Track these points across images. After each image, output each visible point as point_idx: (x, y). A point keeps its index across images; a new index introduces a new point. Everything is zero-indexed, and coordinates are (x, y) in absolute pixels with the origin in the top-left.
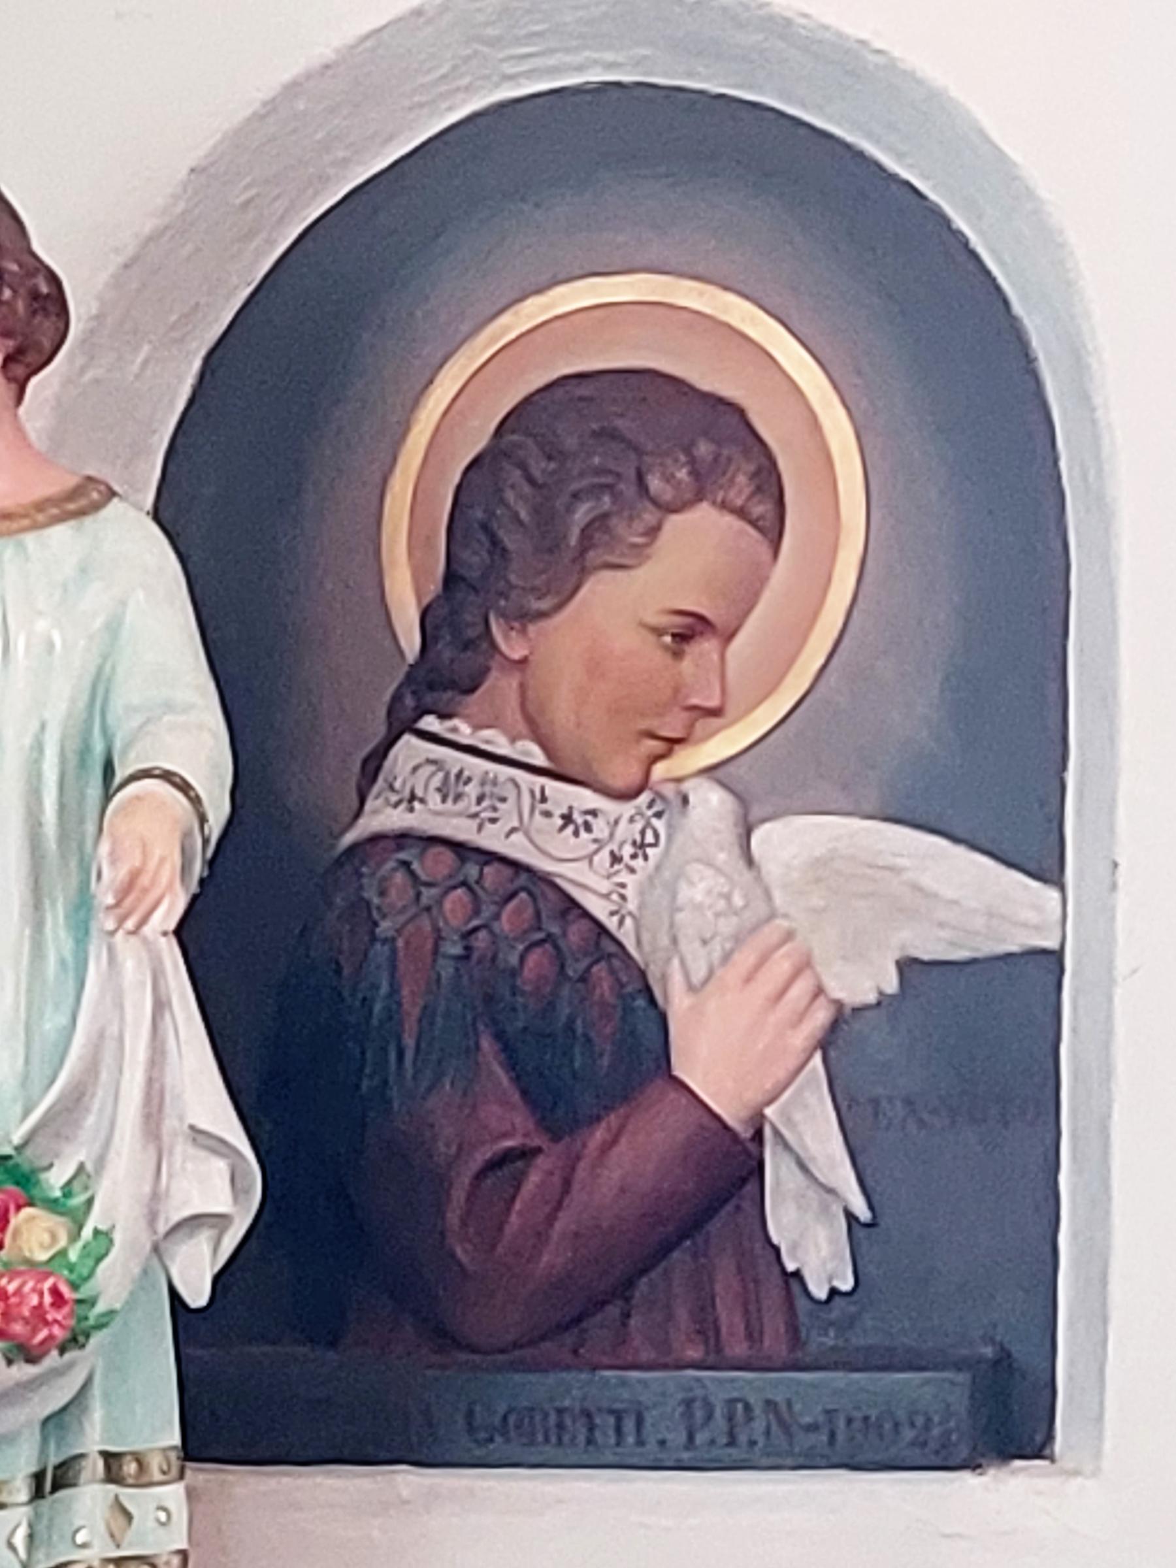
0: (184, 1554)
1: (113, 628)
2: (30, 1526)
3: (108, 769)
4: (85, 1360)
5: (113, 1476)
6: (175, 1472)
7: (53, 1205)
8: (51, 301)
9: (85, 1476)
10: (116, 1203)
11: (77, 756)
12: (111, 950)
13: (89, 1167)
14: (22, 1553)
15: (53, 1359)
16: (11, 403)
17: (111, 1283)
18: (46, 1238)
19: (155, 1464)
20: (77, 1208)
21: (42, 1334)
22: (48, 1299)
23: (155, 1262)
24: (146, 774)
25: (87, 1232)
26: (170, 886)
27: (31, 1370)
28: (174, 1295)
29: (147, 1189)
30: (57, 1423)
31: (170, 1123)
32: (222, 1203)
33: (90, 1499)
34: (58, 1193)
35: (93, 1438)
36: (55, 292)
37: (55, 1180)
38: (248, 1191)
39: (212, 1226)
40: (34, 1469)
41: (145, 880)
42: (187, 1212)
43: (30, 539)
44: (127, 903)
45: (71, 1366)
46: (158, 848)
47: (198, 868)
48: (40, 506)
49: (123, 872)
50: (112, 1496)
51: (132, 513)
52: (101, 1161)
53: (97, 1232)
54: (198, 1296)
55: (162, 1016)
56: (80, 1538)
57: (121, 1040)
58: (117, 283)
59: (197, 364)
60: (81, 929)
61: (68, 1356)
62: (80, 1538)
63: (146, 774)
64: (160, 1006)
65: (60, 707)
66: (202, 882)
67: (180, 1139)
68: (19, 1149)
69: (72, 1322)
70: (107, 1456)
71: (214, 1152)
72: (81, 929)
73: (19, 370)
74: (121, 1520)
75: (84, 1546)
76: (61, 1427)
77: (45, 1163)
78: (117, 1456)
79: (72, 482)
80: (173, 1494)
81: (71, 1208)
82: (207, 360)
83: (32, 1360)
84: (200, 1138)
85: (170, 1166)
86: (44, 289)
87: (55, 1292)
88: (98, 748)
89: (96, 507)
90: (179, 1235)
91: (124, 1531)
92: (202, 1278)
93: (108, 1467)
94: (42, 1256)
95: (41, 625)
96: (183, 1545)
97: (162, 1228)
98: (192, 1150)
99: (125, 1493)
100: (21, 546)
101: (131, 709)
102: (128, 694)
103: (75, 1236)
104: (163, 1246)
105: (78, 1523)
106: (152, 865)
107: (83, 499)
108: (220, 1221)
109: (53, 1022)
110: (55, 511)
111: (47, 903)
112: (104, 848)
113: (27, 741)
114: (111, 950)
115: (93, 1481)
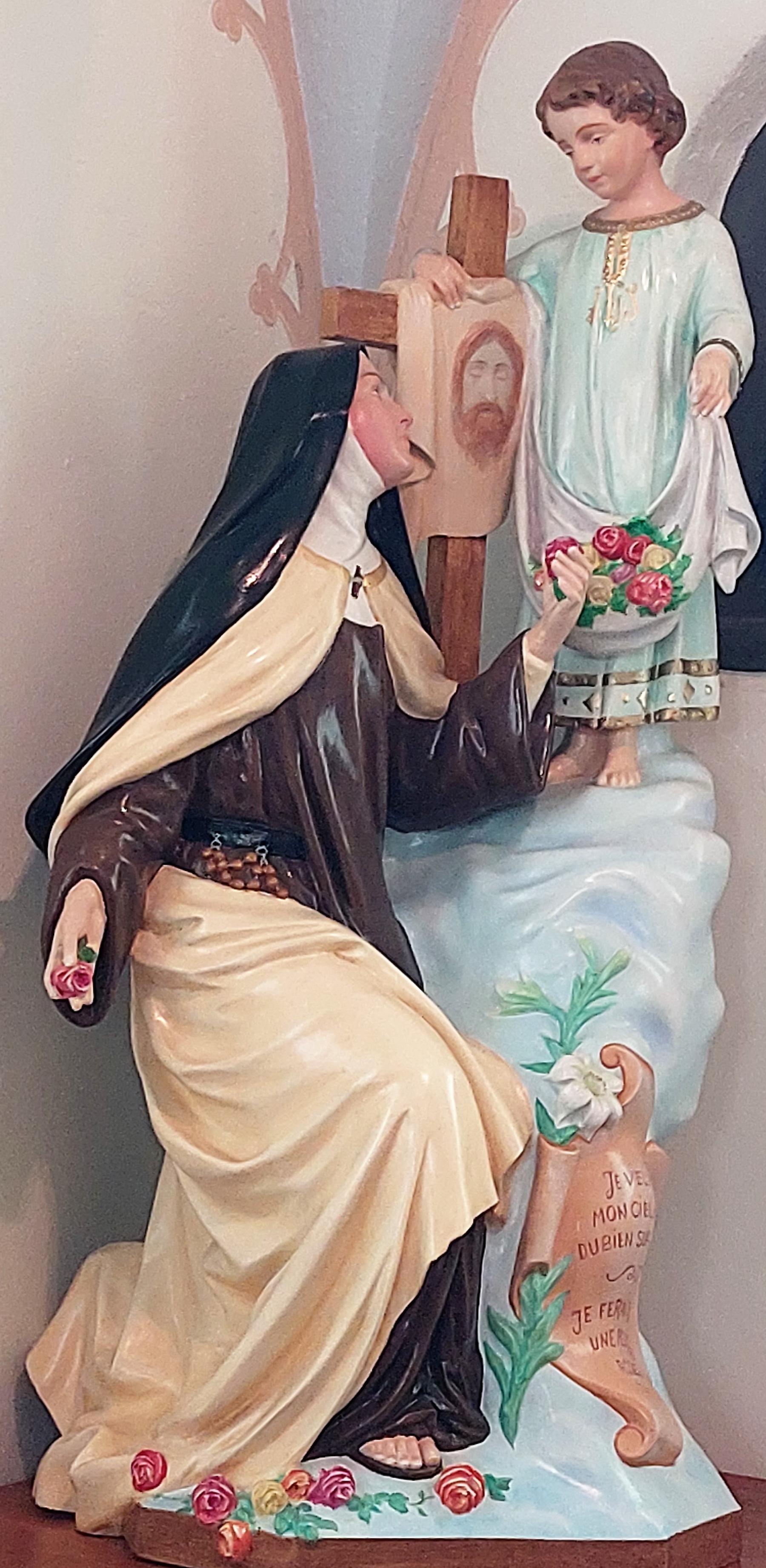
0: (717, 708)
1: (702, 271)
2: (648, 690)
3: (696, 340)
4: (676, 616)
5: (686, 671)
6: (714, 670)
7: (664, 544)
8: (678, 114)
9: (674, 669)
10: (693, 544)
11: (681, 337)
12: (695, 424)
13: (680, 527)
14: (644, 704)
15: (661, 615)
16: (657, 164)
17: (690, 580)
18: (661, 559)
19: (705, 669)
20: (674, 545)
21: (657, 602)
22: (660, 586)
23: (709, 570)
24: (714, 342)
25: (679, 557)
26: (724, 395)
27: (652, 619)
28: (717, 585)
29: (708, 535)
30: (661, 645)
31: (719, 506)
32: (742, 545)
33: (675, 681)
34: (666, 539)
35: (678, 653)
36: (680, 112)
37: (665, 532)
38: (755, 537)
39: (737, 555)
40: (650, 666)
41: (711, 392)
42: (725, 549)
43: (663, 229)
44: (704, 402)
45: (671, 617)
46: (718, 378)
47: (737, 388)
48: (669, 214)
49: (703, 386)
50: (685, 682)
51: (712, 219)
52: (687, 522)
53: (684, 556)
54: (729, 587)
55: (718, 457)
56: (671, 699)
57: (698, 469)
58: (707, 111)
59: (743, 152)
60: (680, 418)
61: (669, 613)
62: (671, 699)
63: (714, 342)
64: (717, 451)
65: (676, 308)
66: (738, 394)
67: (724, 513)
68: (649, 517)
69: (670, 598)
70: (684, 662)
71: (739, 520)
72: (680, 418)
73: (660, 148)
74: (689, 690)
75: (673, 701)
76: (662, 646)
77: (661, 525)
78: (689, 662)
79: (683, 203)
80: (713, 681)
81: (672, 544)
82: (748, 150)
83: (652, 614)
84: (733, 514)
85: (719, 526)
86: (675, 108)
87: (663, 583)
88: (692, 328)
89: (694, 215)
90: (722, 559)
91: (690, 696)
92: (731, 580)
93: (684, 667)
94: (658, 567)
95: (668, 270)
96: (717, 704)
97: (714, 556)
98: (728, 519)
99: (691, 679)
100: (659, 233)
101: (709, 312)
102: (707, 304)
103: (673, 559)
104: (714, 564)
105: (669, 690)
106: (716, 384)
107: (689, 212)
108: (743, 553)
109: (667, 459)
110: (675, 216)
111: (665, 405)
112: (694, 375)
113: (660, 325)
114: (695, 424)
115: (678, 673)
